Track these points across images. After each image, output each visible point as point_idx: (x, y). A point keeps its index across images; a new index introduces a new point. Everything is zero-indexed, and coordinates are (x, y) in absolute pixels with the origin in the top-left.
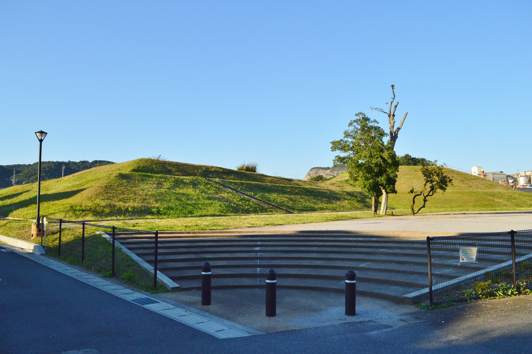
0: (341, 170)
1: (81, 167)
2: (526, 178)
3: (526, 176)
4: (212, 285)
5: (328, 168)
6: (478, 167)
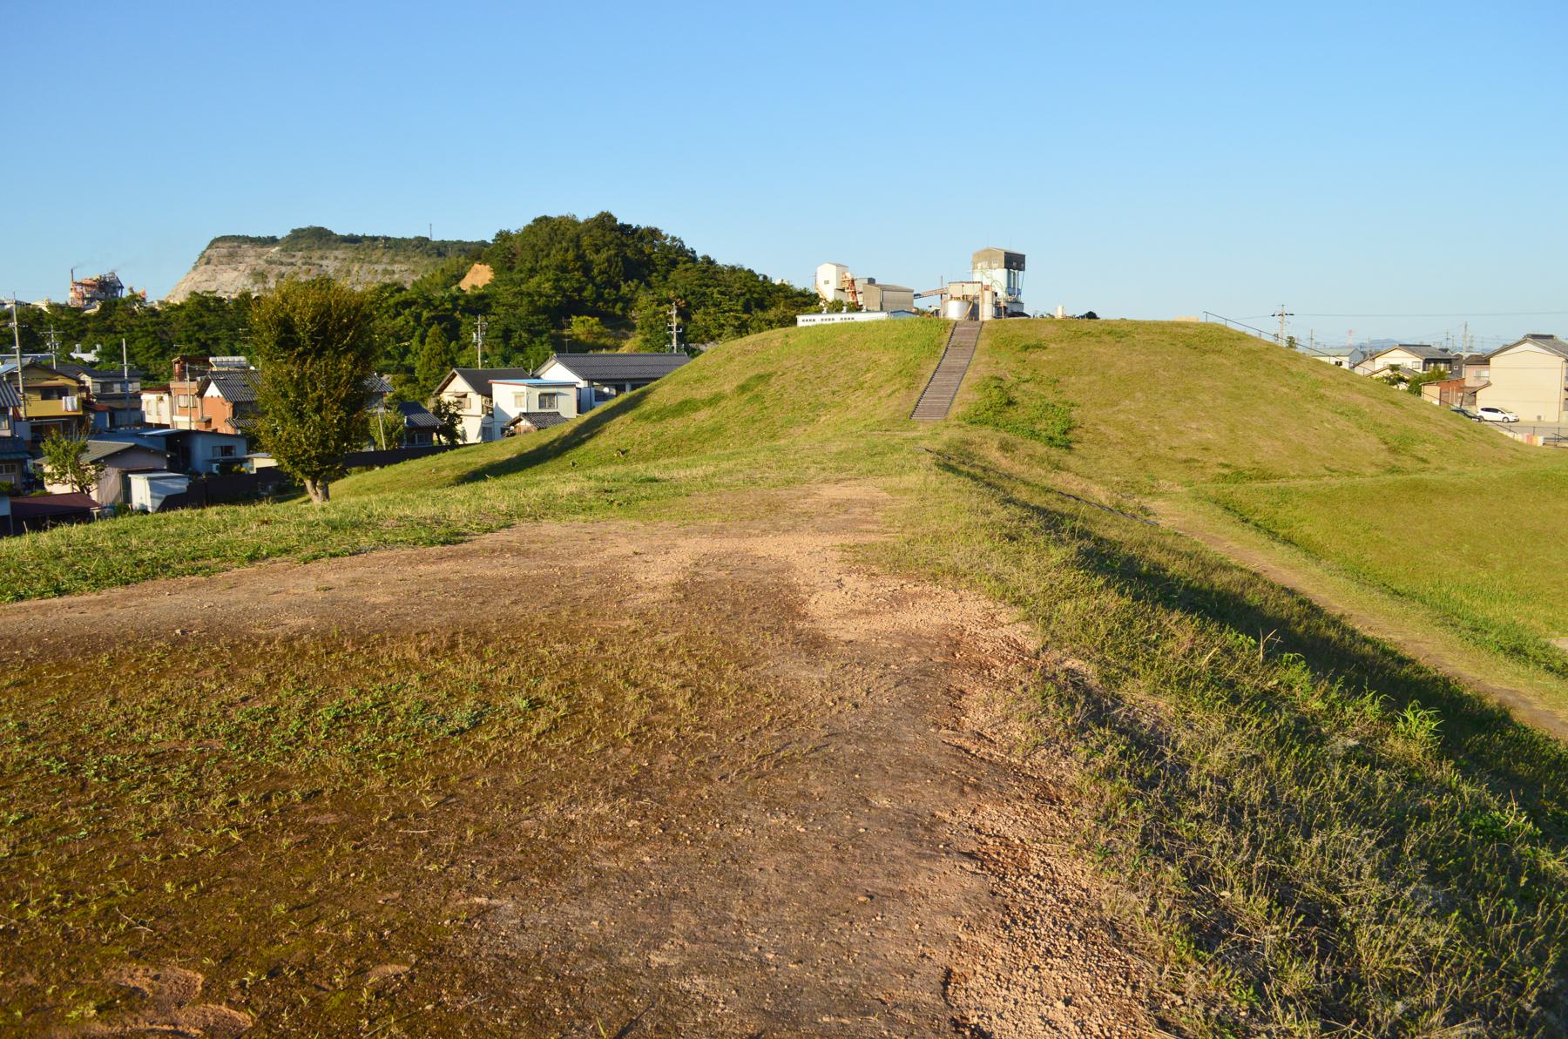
0: (320, 249)
2: (966, 304)
3: (965, 298)
5: (273, 241)
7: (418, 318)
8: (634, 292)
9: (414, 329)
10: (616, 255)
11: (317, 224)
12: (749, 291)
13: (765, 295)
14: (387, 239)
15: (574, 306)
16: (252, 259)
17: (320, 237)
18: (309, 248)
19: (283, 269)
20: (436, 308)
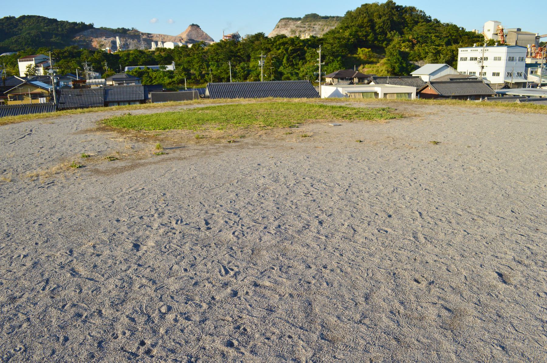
0: (314, 21)
1: (6, 24)
4: (460, 50)
6: (495, 22)
7: (287, 50)
8: (393, 36)
9: (284, 55)
10: (388, 19)
11: (314, 13)
12: (450, 35)
13: (458, 37)
14: (338, 17)
15: (362, 43)
16: (292, 25)
17: (314, 17)
18: (310, 21)
19: (301, 29)
20: (296, 45)
